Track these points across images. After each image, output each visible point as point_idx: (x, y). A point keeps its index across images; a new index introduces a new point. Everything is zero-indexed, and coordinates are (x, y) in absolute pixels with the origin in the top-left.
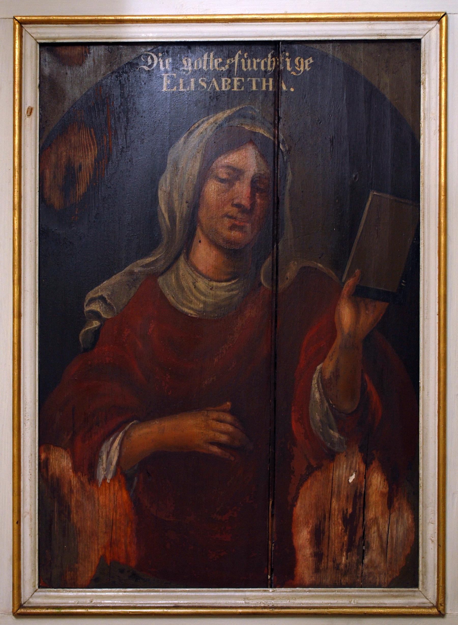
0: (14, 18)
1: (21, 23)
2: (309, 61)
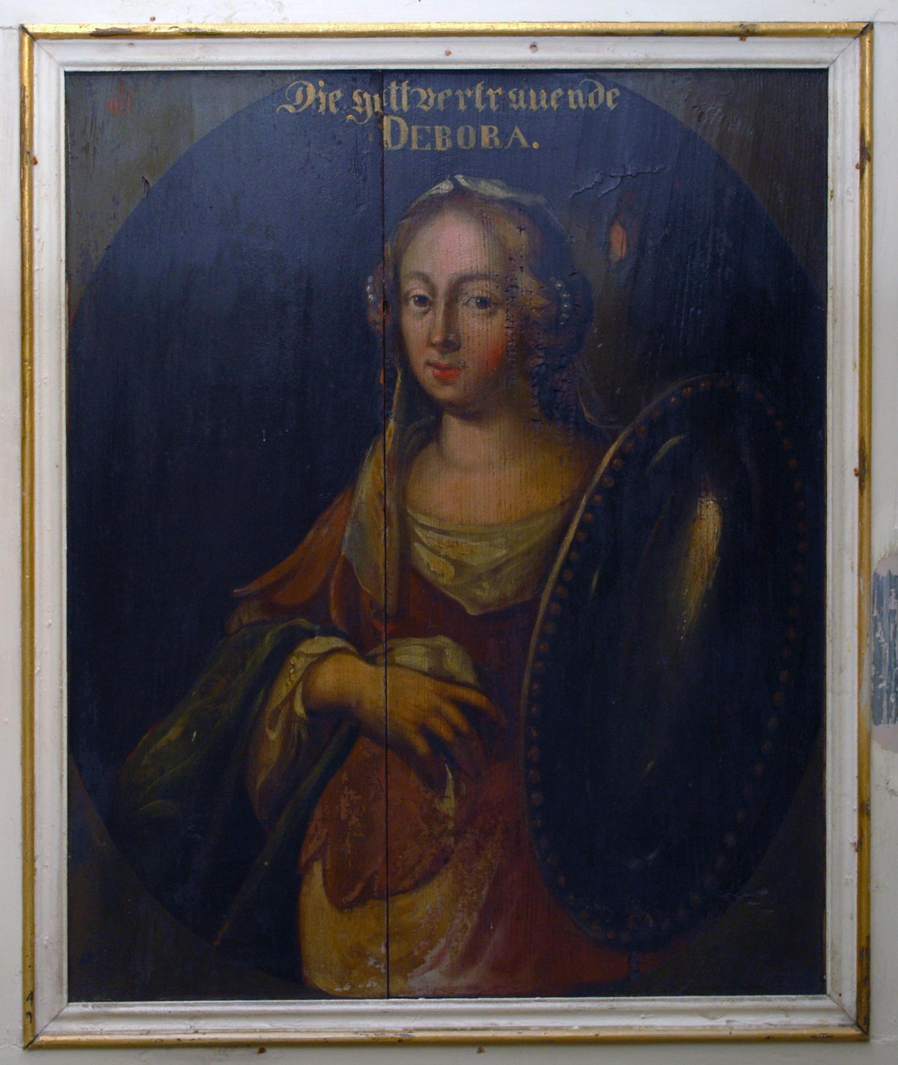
0: (23, 29)
1: (34, 37)
2: (613, 94)
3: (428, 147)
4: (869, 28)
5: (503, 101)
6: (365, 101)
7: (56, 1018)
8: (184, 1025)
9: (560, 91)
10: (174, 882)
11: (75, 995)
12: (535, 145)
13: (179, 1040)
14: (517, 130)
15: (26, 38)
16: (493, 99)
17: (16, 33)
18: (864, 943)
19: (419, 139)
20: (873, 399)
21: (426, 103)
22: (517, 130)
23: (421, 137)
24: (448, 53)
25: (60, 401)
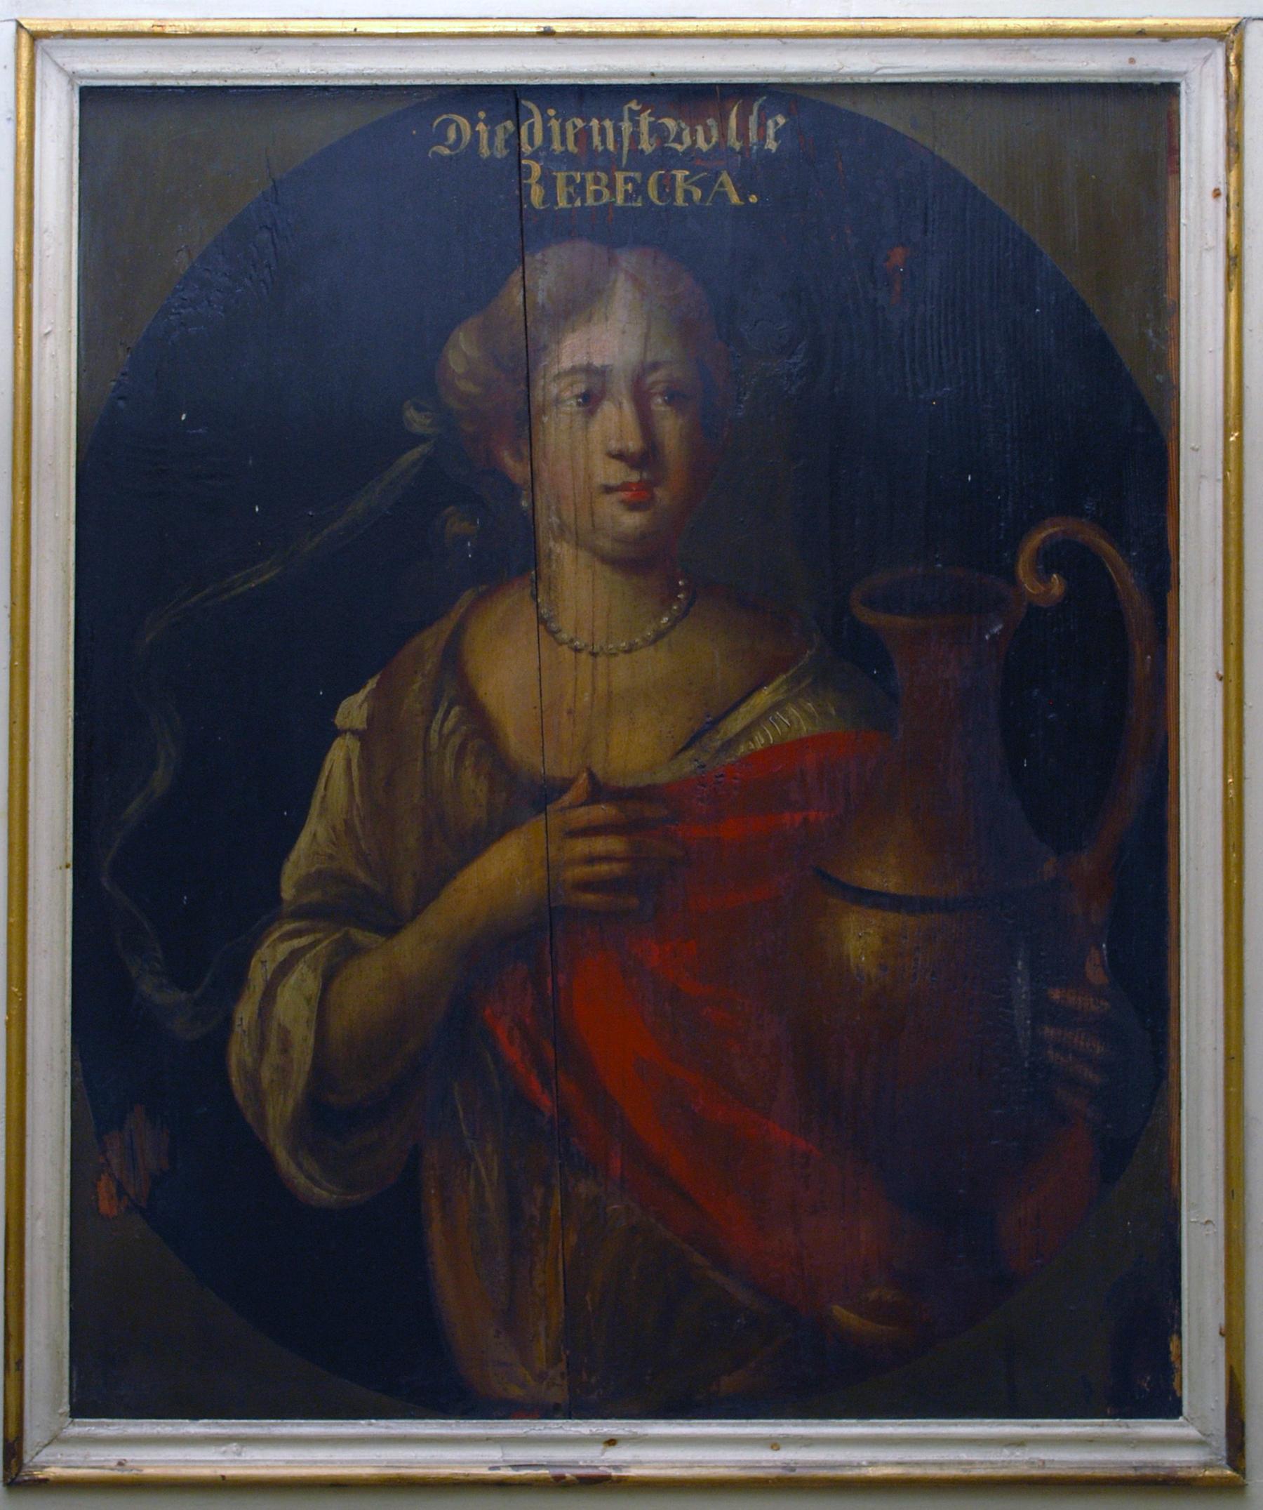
0: (20, 26)
1: (35, 37)
2: (575, 127)
3: (578, 203)
4: (1239, 28)
5: (584, 136)
6: (483, 136)
7: (55, 1440)
8: (494, 1454)
9: (580, 123)
10: (229, 1262)
11: (80, 1409)
12: (753, 199)
13: (223, 1477)
14: (725, 177)
15: (25, 39)
16: (771, 132)
17: (13, 26)
18: (12, 1429)
19: (626, 191)
20: (1247, 602)
21: (679, 139)
22: (725, 177)
23: (630, 186)
24: (1132, 61)
25: (66, 572)
